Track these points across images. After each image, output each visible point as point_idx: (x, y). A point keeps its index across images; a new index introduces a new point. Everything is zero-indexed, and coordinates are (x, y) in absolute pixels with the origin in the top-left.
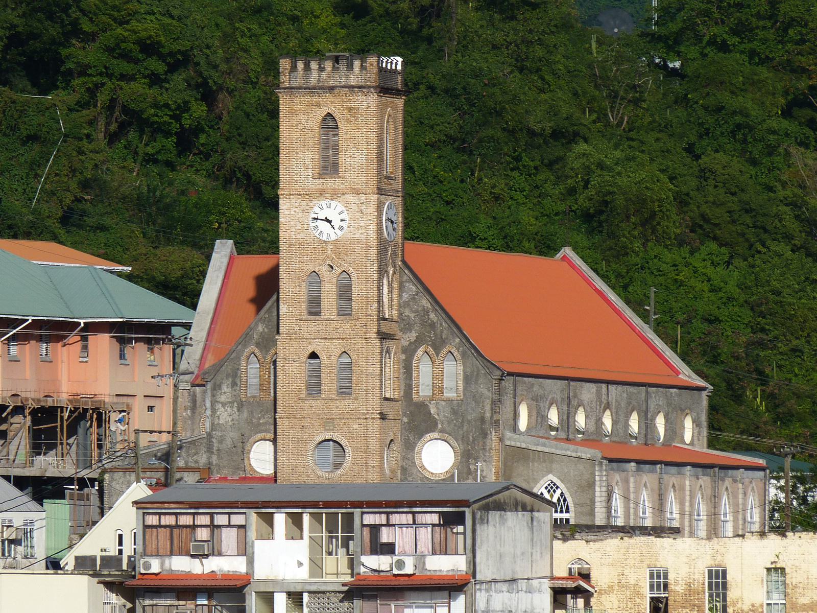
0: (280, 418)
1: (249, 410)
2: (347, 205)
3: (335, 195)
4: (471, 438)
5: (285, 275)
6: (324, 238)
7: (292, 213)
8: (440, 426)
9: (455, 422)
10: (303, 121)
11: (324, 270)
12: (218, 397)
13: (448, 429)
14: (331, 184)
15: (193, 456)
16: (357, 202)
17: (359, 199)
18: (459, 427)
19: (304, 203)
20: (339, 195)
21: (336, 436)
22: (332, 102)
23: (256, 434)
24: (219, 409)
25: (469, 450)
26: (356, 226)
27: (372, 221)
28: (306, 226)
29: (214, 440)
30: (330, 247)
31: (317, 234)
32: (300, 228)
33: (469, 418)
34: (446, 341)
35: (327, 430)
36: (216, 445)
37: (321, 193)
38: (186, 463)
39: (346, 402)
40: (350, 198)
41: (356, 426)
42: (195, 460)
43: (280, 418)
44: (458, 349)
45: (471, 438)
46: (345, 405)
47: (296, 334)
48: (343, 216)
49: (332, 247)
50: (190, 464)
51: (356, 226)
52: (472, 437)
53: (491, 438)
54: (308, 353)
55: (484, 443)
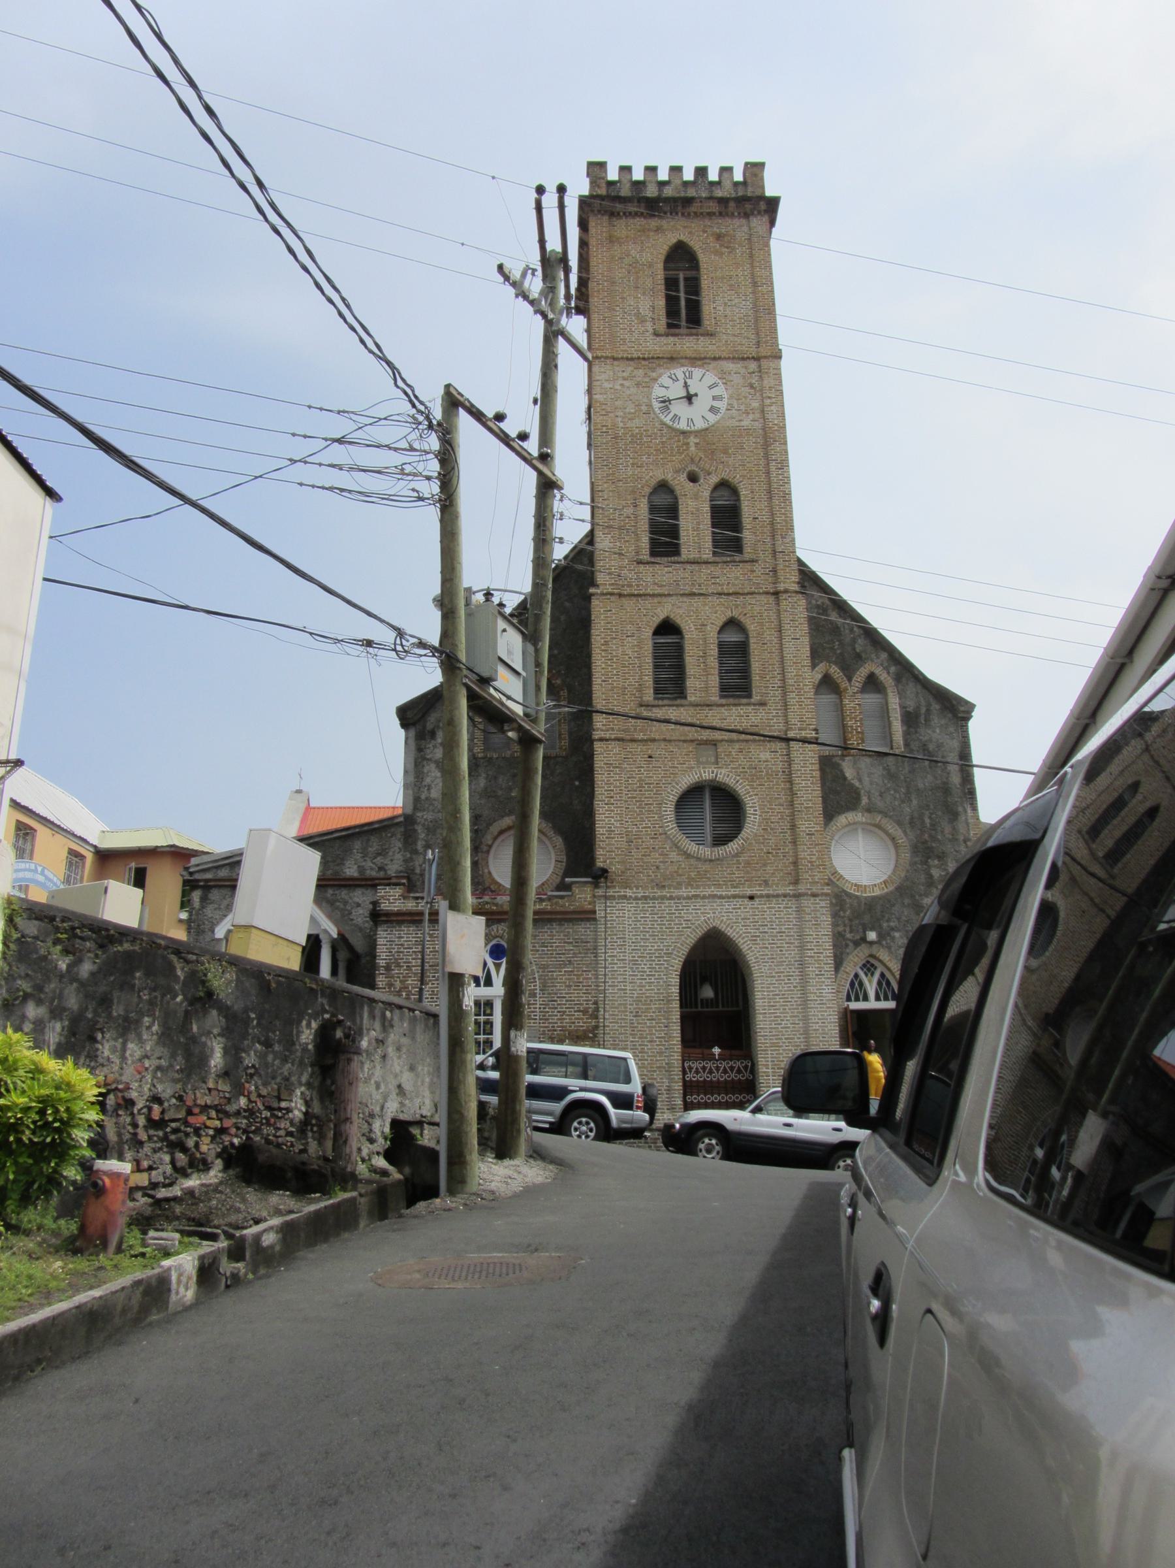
0: (601, 740)
1: (490, 773)
2: (723, 376)
3: (697, 360)
4: (927, 821)
5: (605, 485)
6: (683, 426)
7: (618, 387)
8: (864, 800)
9: (892, 792)
10: (633, 253)
11: (680, 483)
12: (428, 751)
13: (880, 804)
14: (688, 344)
15: (375, 858)
16: (743, 371)
17: (746, 368)
18: (903, 802)
19: (641, 372)
20: (707, 361)
21: (724, 775)
22: (685, 227)
23: (503, 817)
24: (429, 771)
25: (925, 842)
26: (743, 407)
27: (774, 400)
28: (644, 408)
29: (419, 828)
30: (693, 440)
31: (667, 420)
32: (633, 411)
33: (921, 786)
34: (863, 655)
35: (702, 763)
36: (422, 836)
37: (673, 359)
38: (361, 869)
39: (742, 710)
40: (729, 366)
41: (763, 756)
42: (379, 865)
43: (601, 740)
44: (887, 669)
45: (927, 821)
46: (736, 715)
47: (630, 586)
48: (717, 391)
49: (697, 441)
50: (368, 872)
51: (743, 407)
52: (930, 818)
53: (966, 819)
54: (656, 621)
55: (954, 829)
